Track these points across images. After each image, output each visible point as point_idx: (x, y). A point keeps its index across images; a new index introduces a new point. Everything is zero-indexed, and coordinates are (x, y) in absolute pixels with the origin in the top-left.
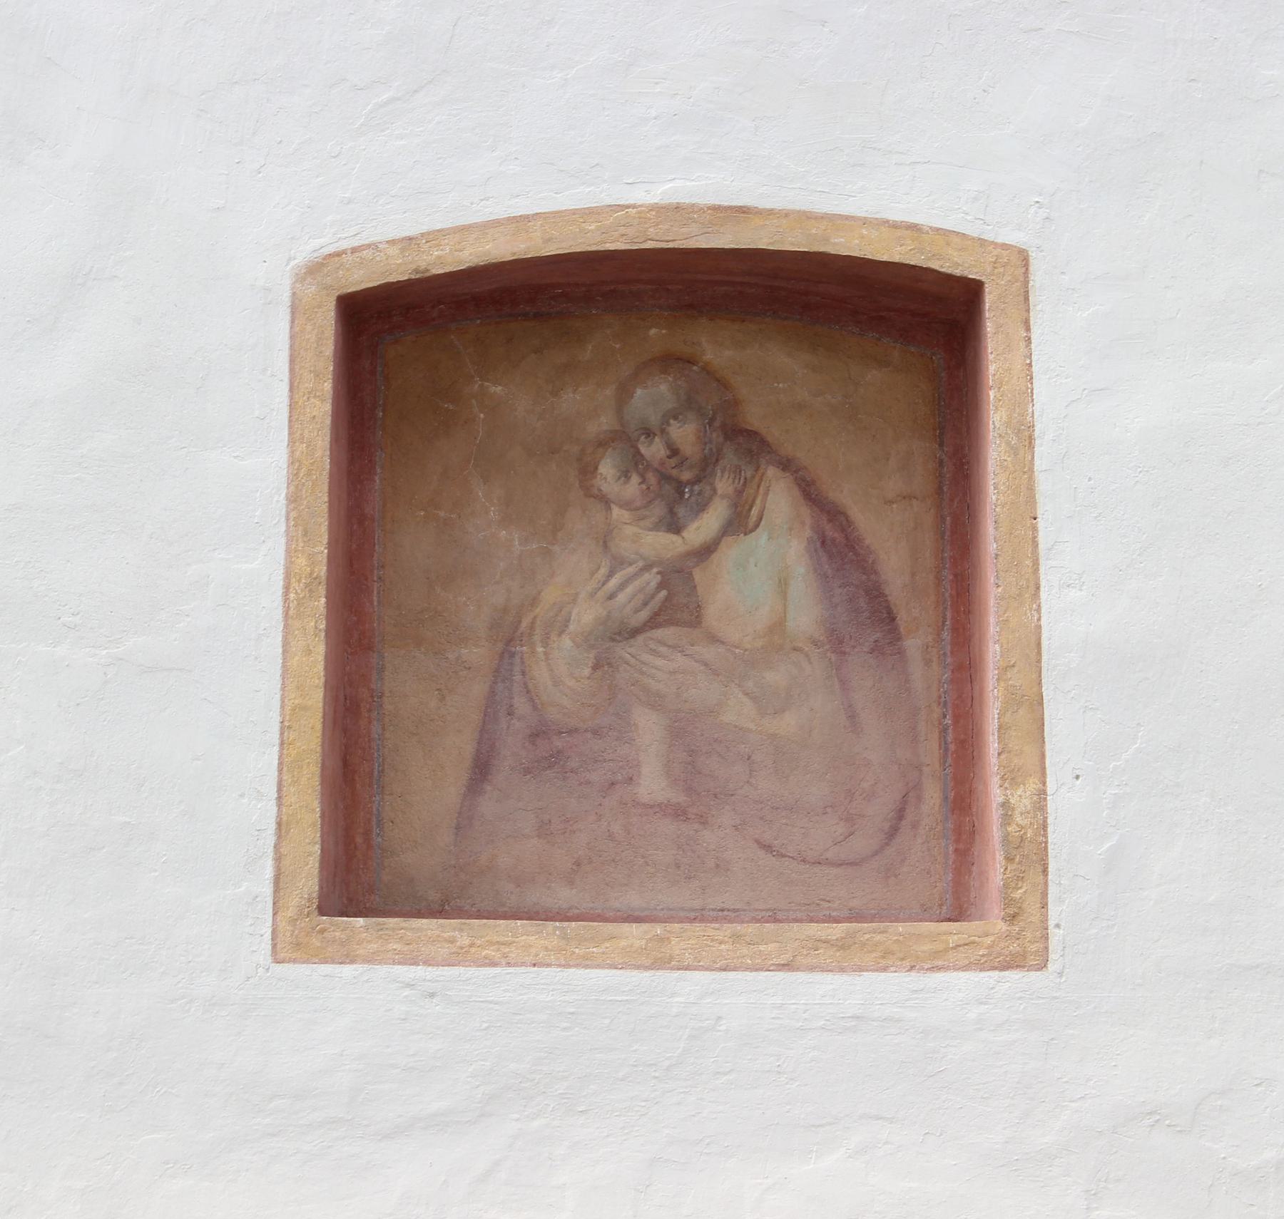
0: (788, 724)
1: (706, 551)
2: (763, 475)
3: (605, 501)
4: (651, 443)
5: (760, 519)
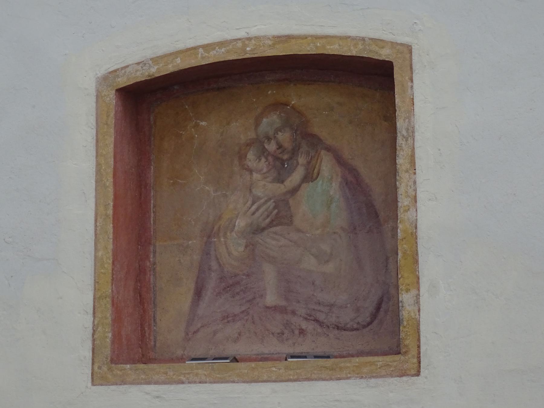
0: (330, 268)
1: (294, 191)
2: (319, 154)
3: (251, 171)
4: (269, 144)
5: (318, 174)
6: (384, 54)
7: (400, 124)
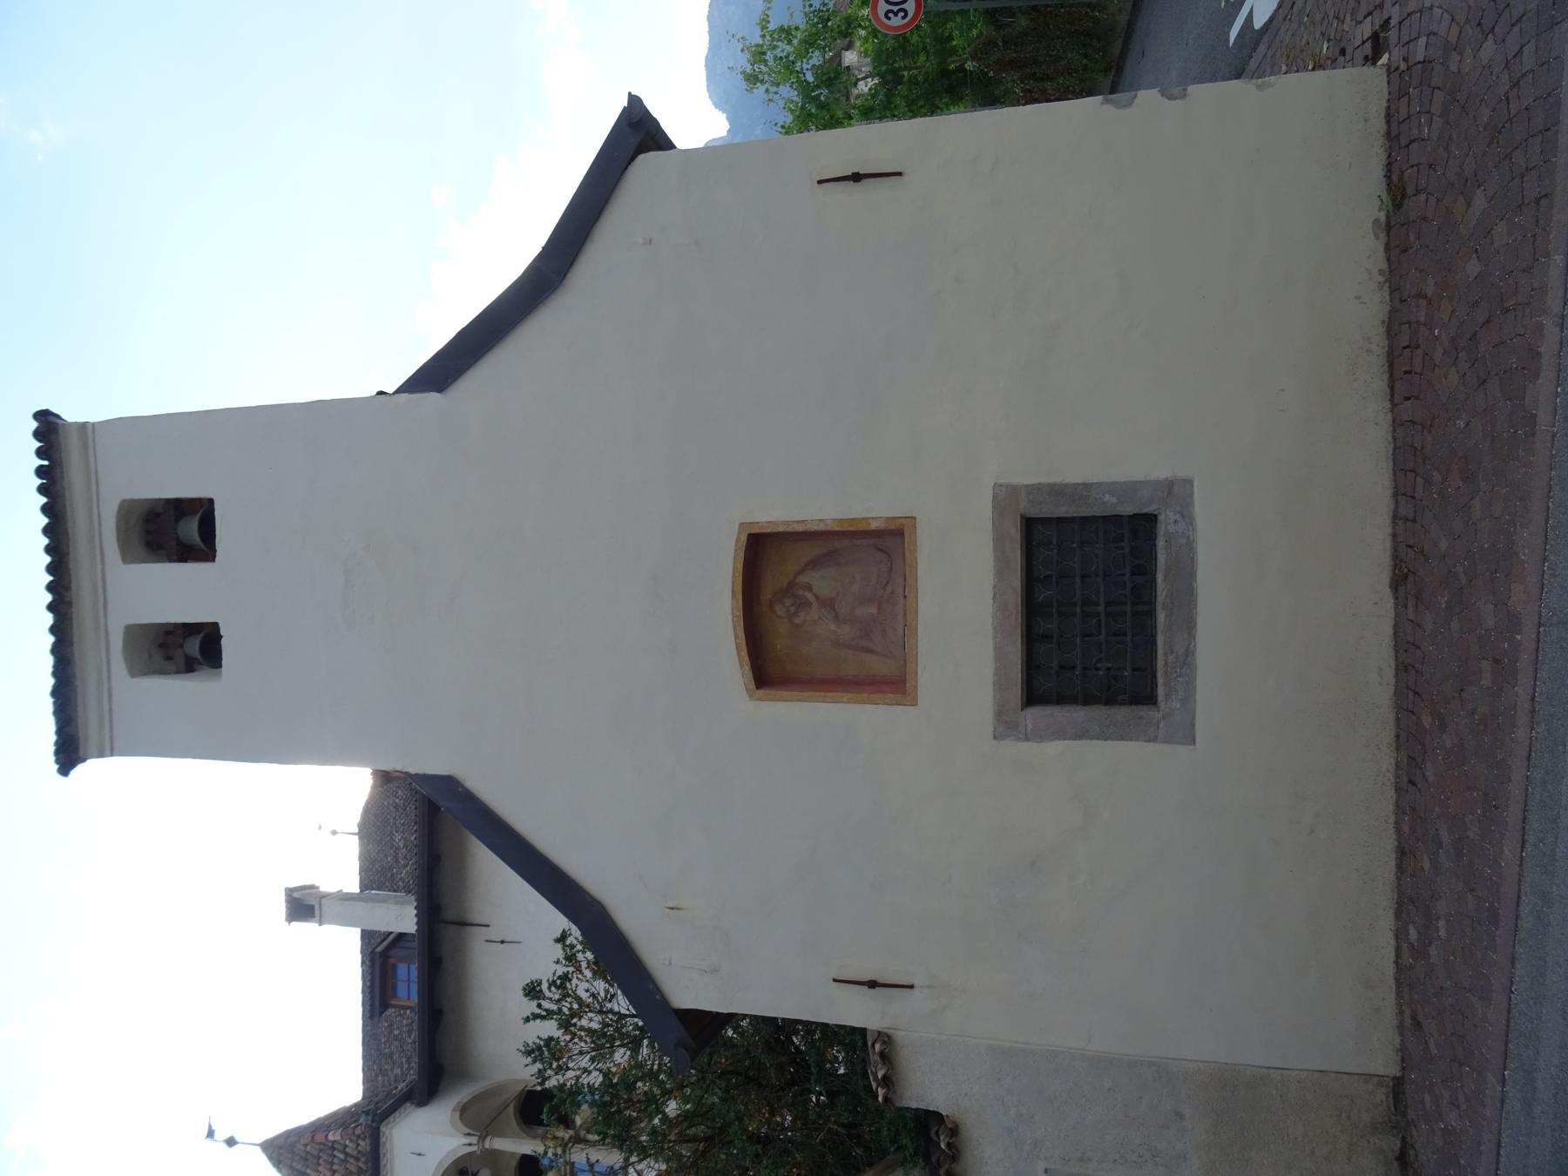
1: (817, 597)
6: (744, 538)
7: (781, 529)
